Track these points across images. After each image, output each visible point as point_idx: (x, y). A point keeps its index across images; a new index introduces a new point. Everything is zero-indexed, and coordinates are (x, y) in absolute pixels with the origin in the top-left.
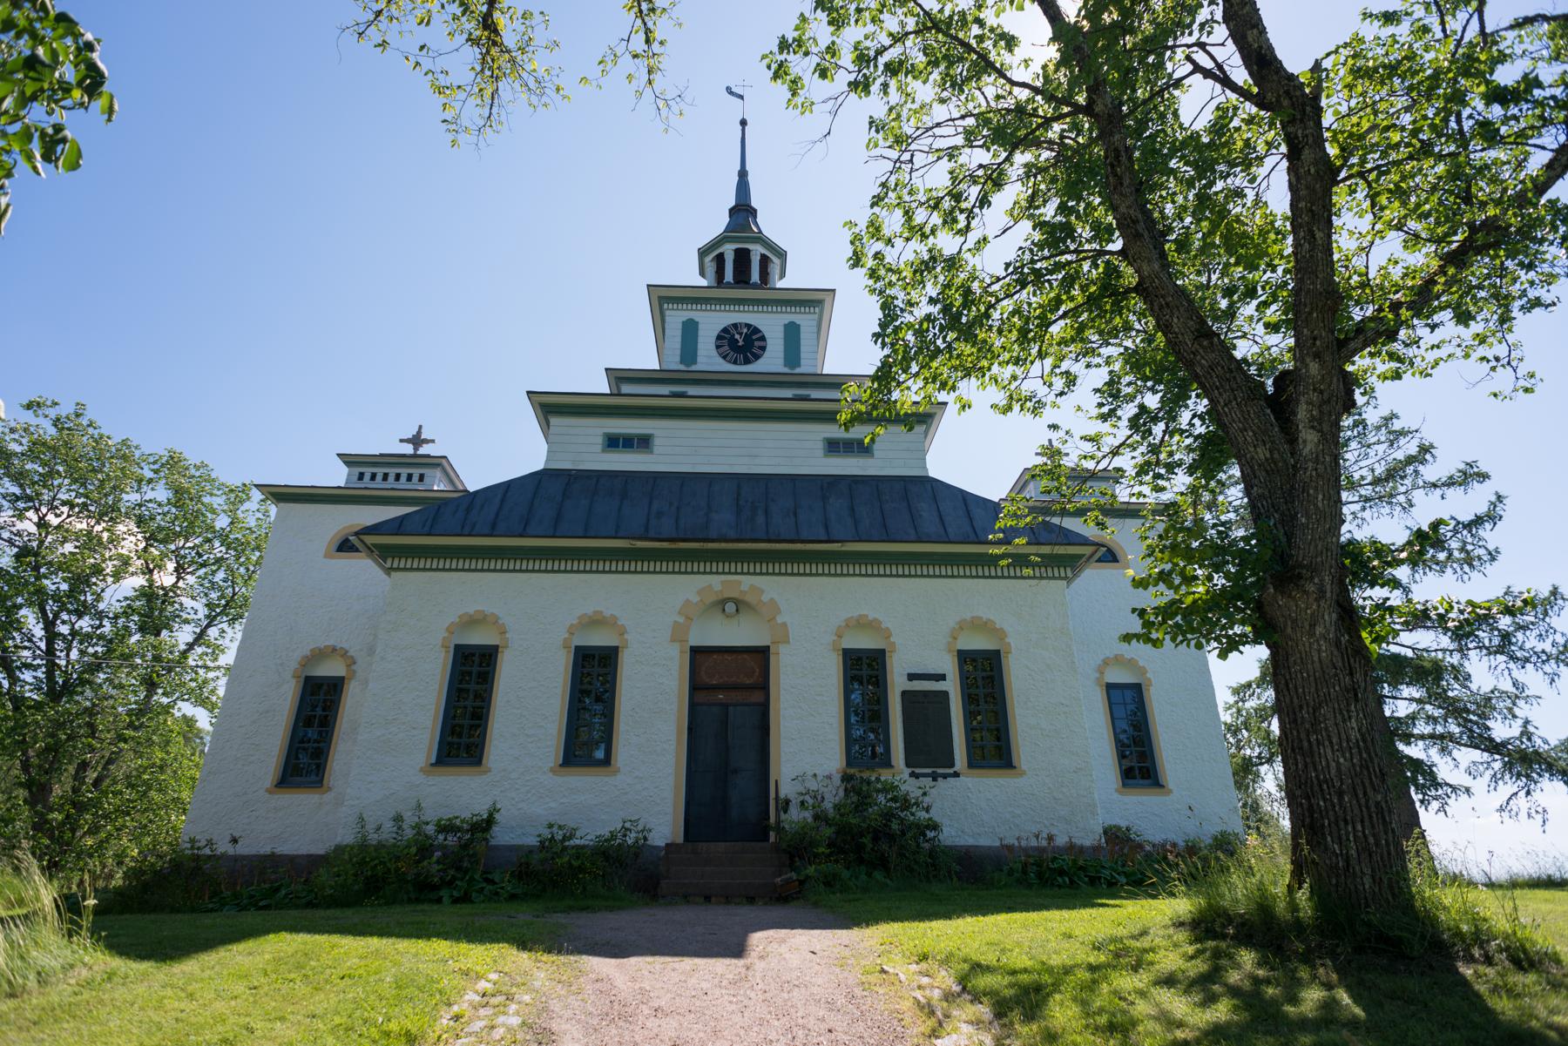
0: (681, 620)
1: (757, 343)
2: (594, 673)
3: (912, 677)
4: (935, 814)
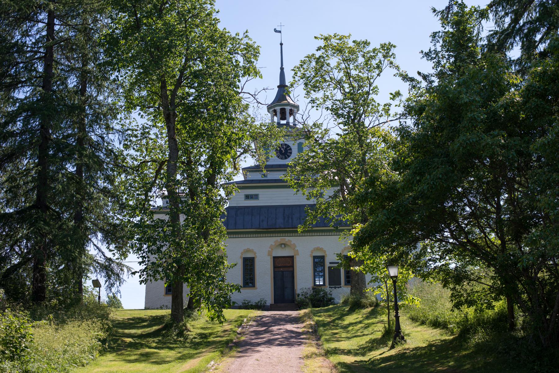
0: (270, 250)
1: (289, 151)
2: (249, 265)
3: (330, 263)
4: (333, 296)
